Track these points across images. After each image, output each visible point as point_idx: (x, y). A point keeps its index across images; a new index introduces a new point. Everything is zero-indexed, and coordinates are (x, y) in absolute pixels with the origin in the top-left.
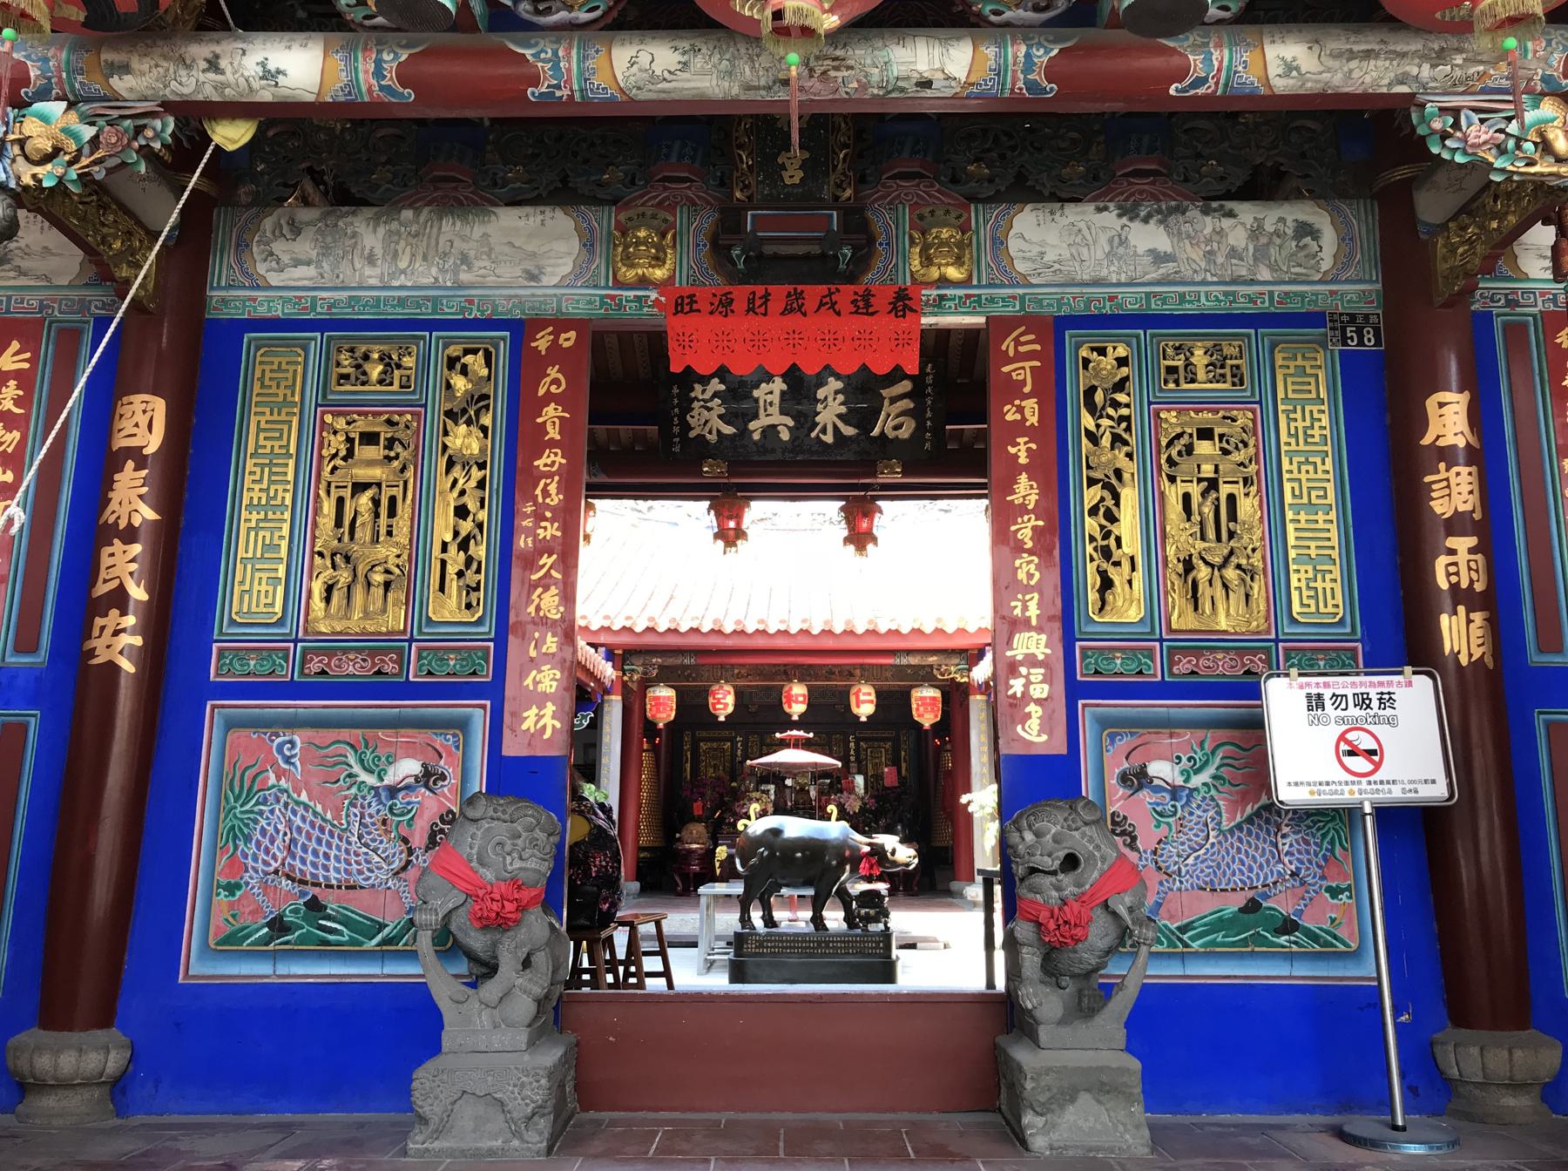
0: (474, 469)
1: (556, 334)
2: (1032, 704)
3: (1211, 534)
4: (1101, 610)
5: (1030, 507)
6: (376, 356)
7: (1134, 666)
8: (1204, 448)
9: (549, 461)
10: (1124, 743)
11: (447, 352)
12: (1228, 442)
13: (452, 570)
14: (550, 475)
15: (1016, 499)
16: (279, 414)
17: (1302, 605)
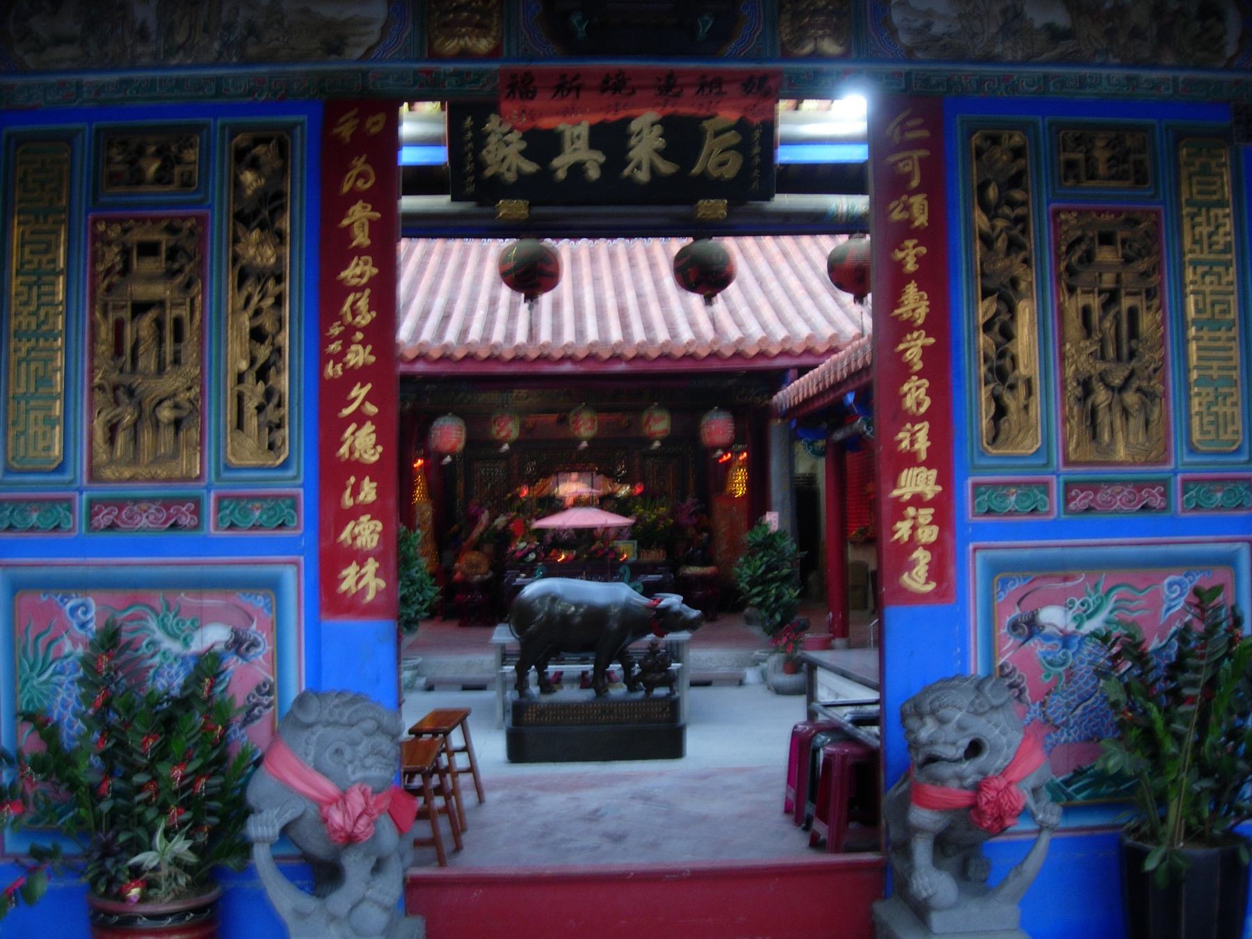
0: (271, 284)
1: (362, 117)
2: (921, 549)
3: (1111, 352)
4: (995, 438)
5: (920, 322)
6: (152, 149)
7: (1028, 504)
8: (1105, 255)
9: (358, 271)
10: (1016, 587)
11: (235, 141)
12: (1130, 246)
13: (250, 406)
14: (358, 289)
15: (903, 312)
16: (45, 222)
17: (1203, 432)
